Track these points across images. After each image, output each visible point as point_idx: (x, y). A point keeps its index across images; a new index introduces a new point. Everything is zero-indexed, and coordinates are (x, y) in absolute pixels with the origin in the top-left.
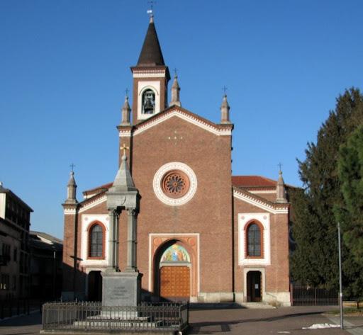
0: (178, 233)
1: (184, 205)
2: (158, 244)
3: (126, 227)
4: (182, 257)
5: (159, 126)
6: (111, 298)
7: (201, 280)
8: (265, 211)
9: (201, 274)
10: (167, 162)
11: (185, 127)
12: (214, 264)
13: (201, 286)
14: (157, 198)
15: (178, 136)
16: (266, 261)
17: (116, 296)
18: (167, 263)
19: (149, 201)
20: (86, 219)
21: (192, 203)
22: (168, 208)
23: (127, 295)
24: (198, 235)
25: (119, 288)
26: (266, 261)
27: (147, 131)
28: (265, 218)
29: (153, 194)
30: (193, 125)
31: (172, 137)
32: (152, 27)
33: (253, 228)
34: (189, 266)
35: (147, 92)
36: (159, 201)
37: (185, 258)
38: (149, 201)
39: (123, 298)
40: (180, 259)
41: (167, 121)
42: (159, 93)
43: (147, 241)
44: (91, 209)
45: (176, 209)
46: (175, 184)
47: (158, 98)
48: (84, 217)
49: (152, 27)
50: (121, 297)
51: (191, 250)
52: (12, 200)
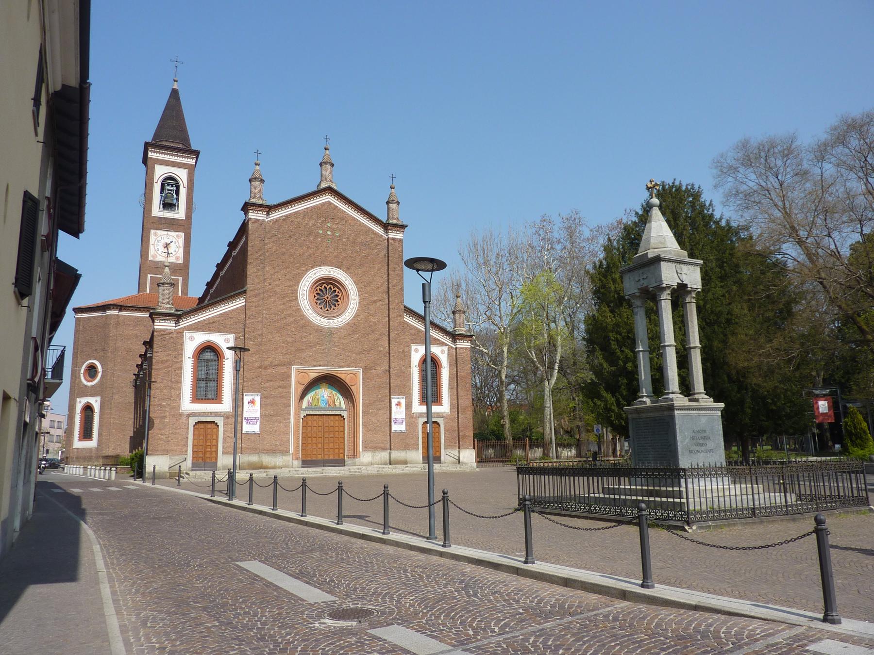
0: (333, 366)
1: (341, 328)
2: (347, 379)
3: (692, 318)
4: (334, 402)
5: (306, 213)
6: (690, 452)
7: (365, 435)
8: (443, 344)
9: (365, 425)
10: (317, 266)
11: (342, 219)
12: (381, 412)
13: (364, 442)
14: (303, 315)
15: (332, 230)
16: (443, 408)
17: (697, 448)
18: (149, 422)
19: (292, 318)
20: (192, 339)
21: (352, 325)
22: (319, 330)
23: (710, 445)
24: (360, 370)
25: (698, 432)
26: (443, 408)
27: (288, 217)
28: (443, 352)
29: (298, 309)
30: (353, 219)
31: (325, 231)
32: (175, 94)
33: (430, 364)
34: (344, 414)
35: (170, 181)
36: (307, 320)
37: (337, 403)
38: (292, 318)
39: (707, 451)
40: (331, 405)
41: (317, 206)
42: (186, 185)
43: (289, 376)
44: (198, 323)
45: (330, 332)
46: (328, 297)
47: (183, 191)
48: (187, 335)
49: (175, 94)
50: (703, 448)
51: (345, 390)
52: (406, 226)
